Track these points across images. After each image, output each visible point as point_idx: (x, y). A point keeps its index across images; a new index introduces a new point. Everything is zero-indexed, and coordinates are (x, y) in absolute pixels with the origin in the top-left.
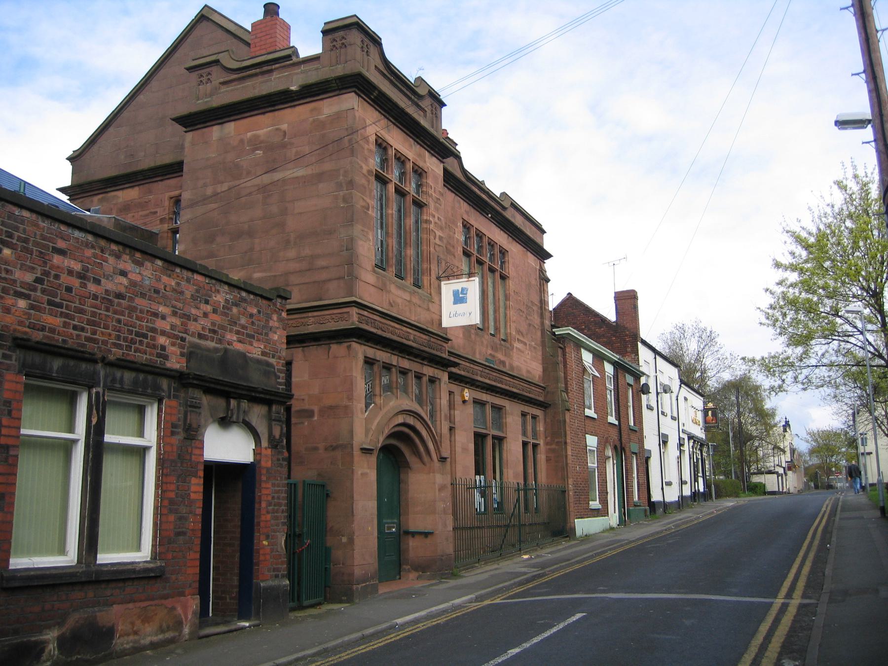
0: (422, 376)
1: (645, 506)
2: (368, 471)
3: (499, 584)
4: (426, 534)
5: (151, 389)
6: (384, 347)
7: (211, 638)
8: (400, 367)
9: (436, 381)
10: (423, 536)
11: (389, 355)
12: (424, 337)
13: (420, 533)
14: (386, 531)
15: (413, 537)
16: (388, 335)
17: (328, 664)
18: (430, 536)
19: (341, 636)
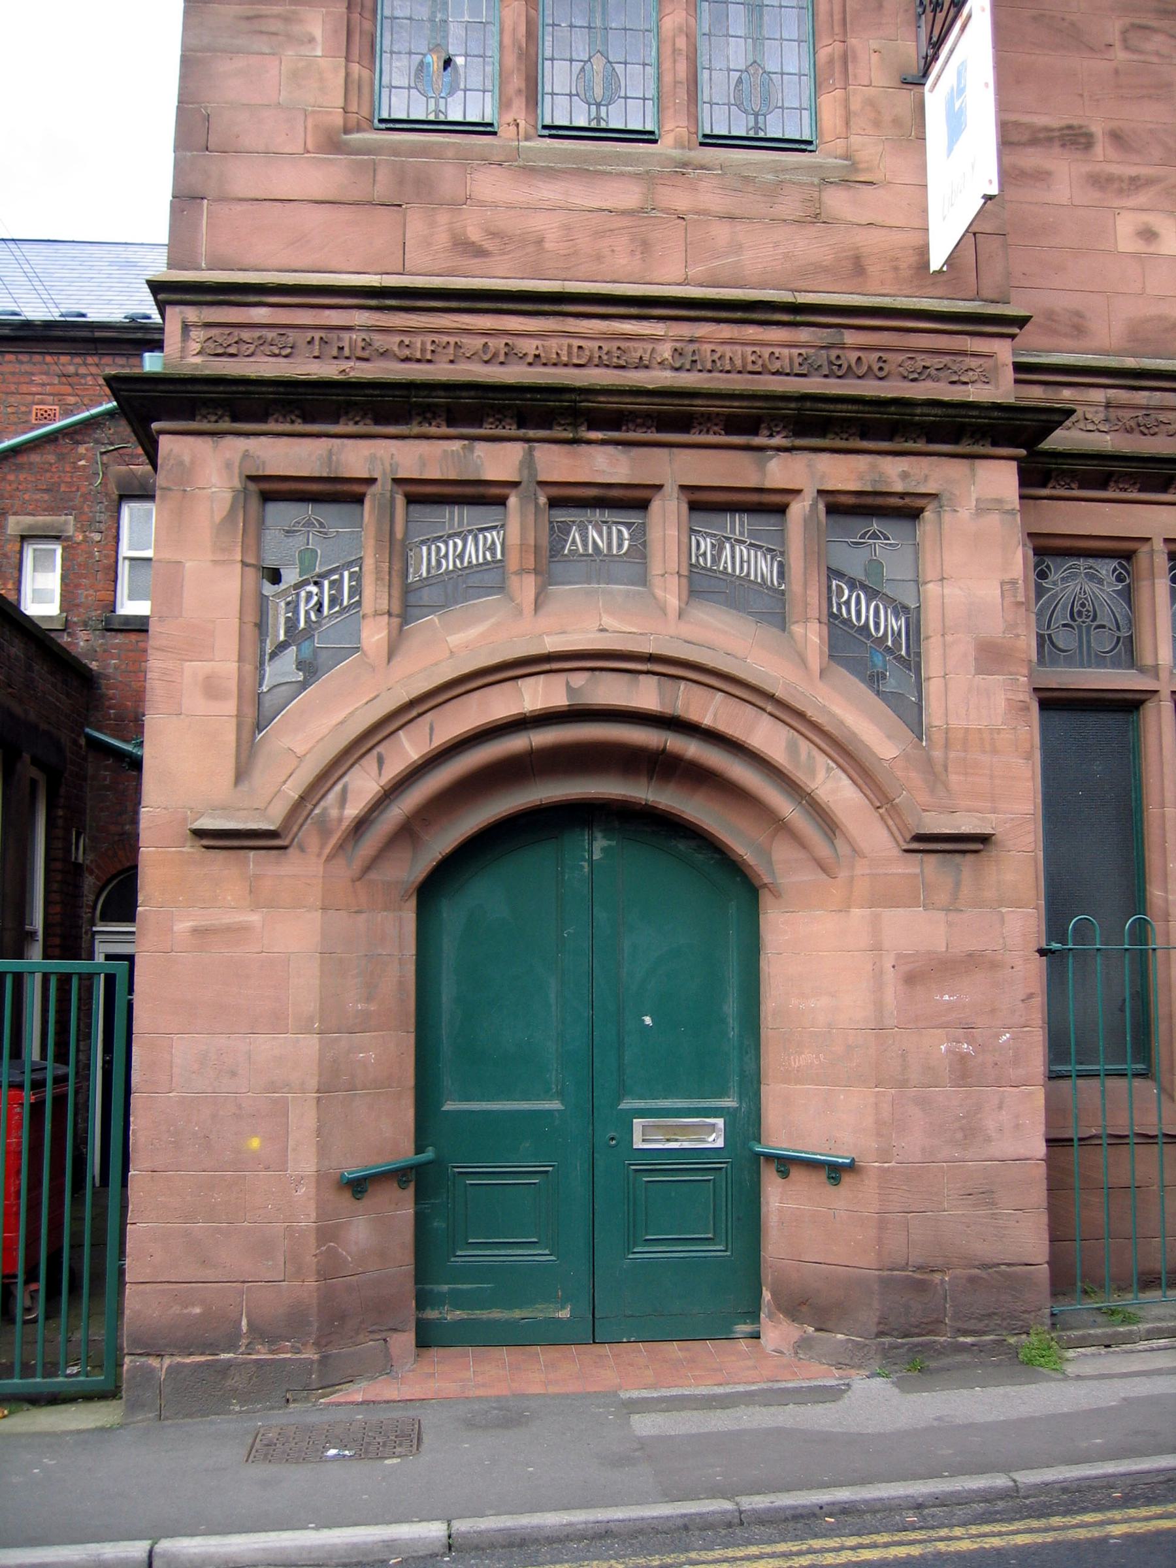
0: (919, 503)
1: (349, 1253)
2: (255, 918)
3: (841, 1485)
4: (835, 1172)
5: (110, 714)
6: (307, 418)
7: (391, 1404)
8: (542, 484)
9: (921, 510)
10: (822, 1176)
11: (456, 445)
12: (804, 335)
13: (812, 1165)
14: (638, 1144)
15: (784, 1174)
16: (441, 371)
17: (805, 1561)
18: (847, 1179)
19: (864, 1481)
